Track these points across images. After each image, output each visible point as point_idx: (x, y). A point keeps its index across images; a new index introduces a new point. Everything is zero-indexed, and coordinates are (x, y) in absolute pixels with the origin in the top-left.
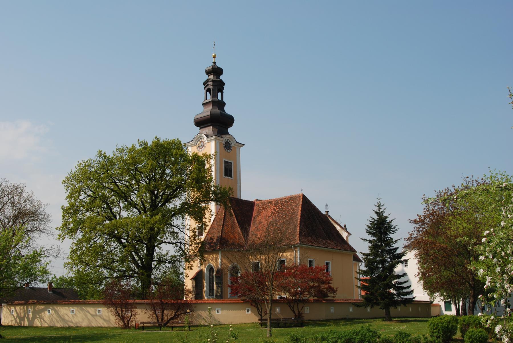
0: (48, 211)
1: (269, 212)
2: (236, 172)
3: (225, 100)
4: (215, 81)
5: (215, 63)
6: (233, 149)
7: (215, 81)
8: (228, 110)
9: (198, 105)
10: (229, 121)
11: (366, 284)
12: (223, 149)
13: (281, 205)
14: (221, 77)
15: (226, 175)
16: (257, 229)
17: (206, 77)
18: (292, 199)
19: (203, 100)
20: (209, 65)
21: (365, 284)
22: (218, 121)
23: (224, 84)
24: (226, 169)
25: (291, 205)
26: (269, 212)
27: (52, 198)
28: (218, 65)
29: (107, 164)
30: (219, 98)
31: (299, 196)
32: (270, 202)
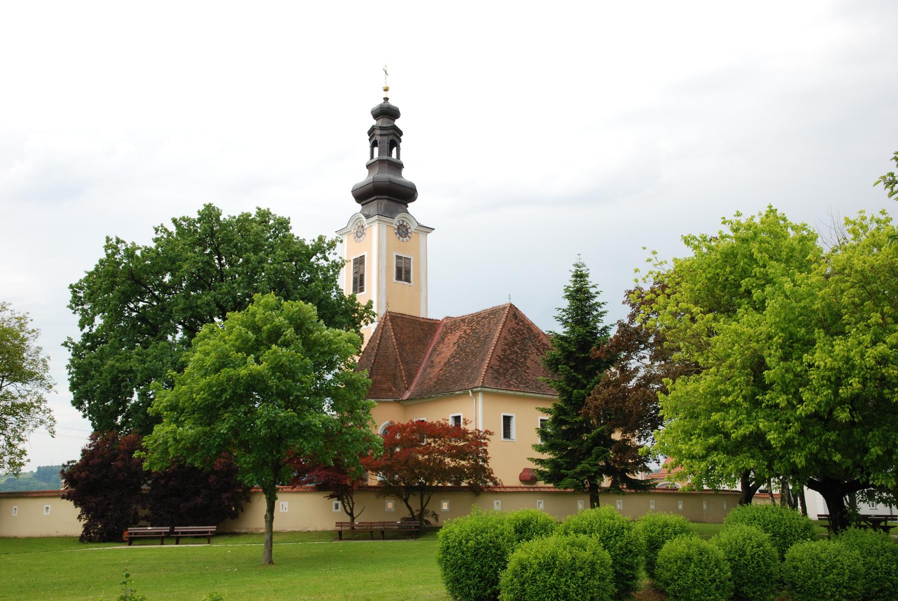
0: (873, 211)
1: (453, 338)
2: (418, 273)
3: (403, 159)
4: (386, 127)
5: (386, 99)
6: (413, 236)
7: (386, 127)
8: (408, 175)
9: (356, 166)
10: (406, 194)
11: (542, 469)
12: (394, 237)
13: (477, 324)
14: (398, 123)
15: (399, 277)
16: (432, 364)
17: (374, 122)
18: (493, 313)
19: (367, 159)
20: (378, 102)
21: (539, 467)
22: (387, 193)
23: (400, 133)
24: (399, 270)
25: (489, 323)
26: (453, 338)
27: (55, 333)
28: (392, 102)
29: (91, 274)
30: (394, 156)
31: (505, 308)
32: (463, 320)
